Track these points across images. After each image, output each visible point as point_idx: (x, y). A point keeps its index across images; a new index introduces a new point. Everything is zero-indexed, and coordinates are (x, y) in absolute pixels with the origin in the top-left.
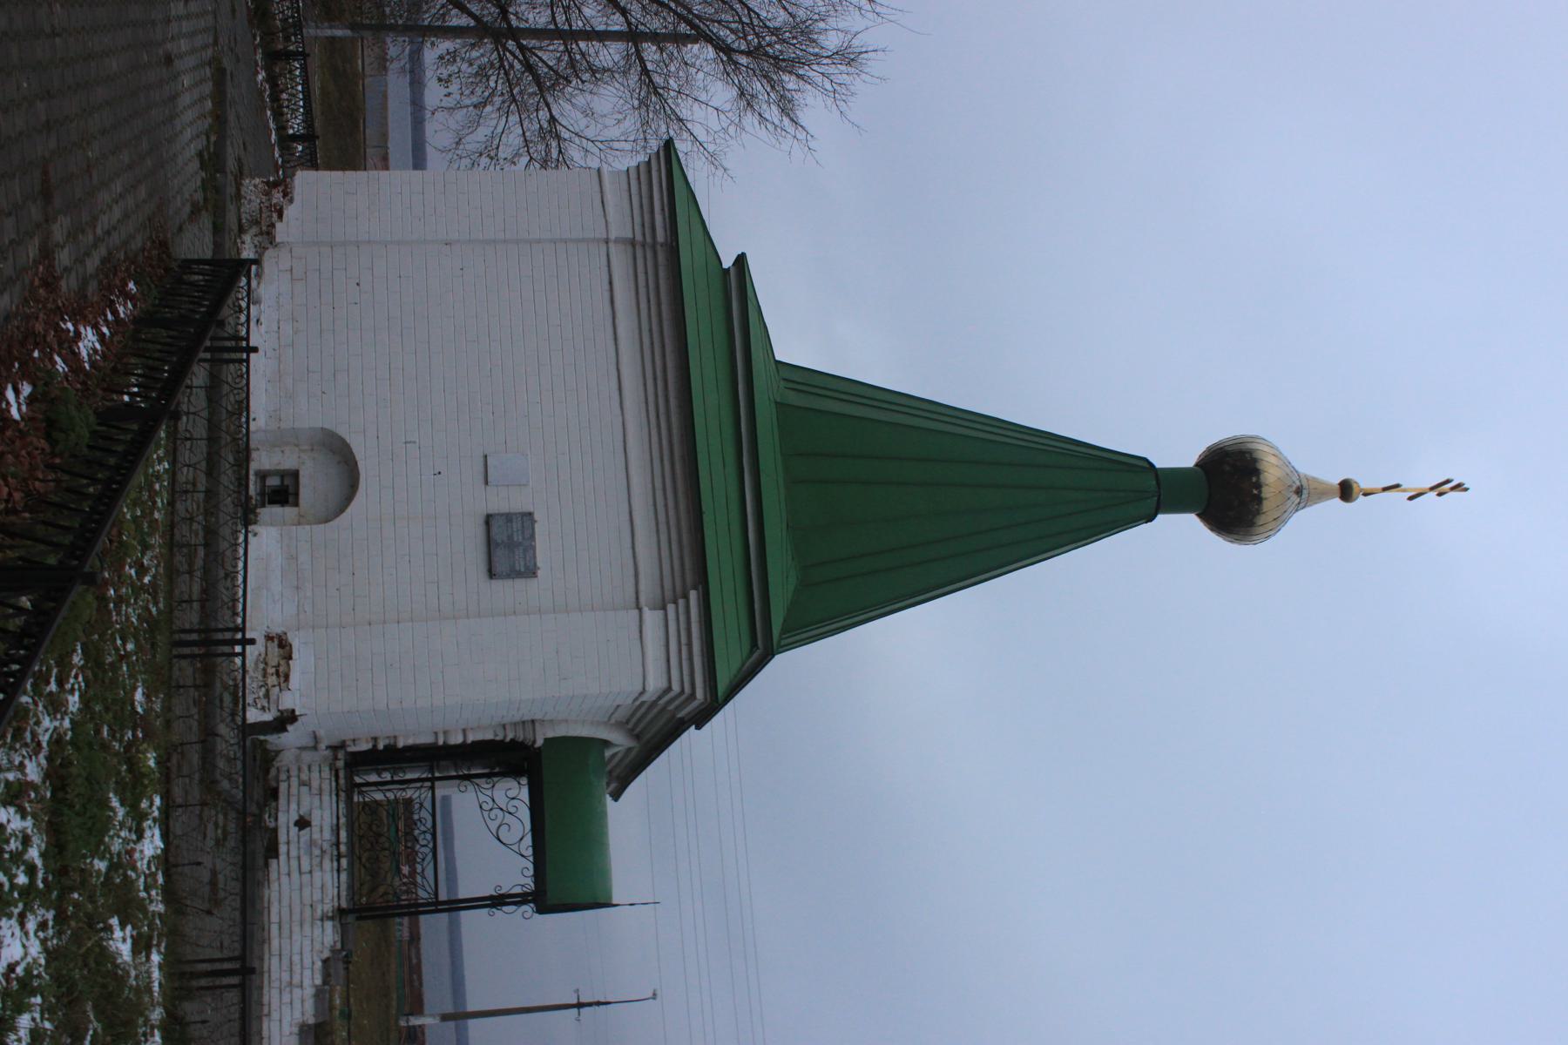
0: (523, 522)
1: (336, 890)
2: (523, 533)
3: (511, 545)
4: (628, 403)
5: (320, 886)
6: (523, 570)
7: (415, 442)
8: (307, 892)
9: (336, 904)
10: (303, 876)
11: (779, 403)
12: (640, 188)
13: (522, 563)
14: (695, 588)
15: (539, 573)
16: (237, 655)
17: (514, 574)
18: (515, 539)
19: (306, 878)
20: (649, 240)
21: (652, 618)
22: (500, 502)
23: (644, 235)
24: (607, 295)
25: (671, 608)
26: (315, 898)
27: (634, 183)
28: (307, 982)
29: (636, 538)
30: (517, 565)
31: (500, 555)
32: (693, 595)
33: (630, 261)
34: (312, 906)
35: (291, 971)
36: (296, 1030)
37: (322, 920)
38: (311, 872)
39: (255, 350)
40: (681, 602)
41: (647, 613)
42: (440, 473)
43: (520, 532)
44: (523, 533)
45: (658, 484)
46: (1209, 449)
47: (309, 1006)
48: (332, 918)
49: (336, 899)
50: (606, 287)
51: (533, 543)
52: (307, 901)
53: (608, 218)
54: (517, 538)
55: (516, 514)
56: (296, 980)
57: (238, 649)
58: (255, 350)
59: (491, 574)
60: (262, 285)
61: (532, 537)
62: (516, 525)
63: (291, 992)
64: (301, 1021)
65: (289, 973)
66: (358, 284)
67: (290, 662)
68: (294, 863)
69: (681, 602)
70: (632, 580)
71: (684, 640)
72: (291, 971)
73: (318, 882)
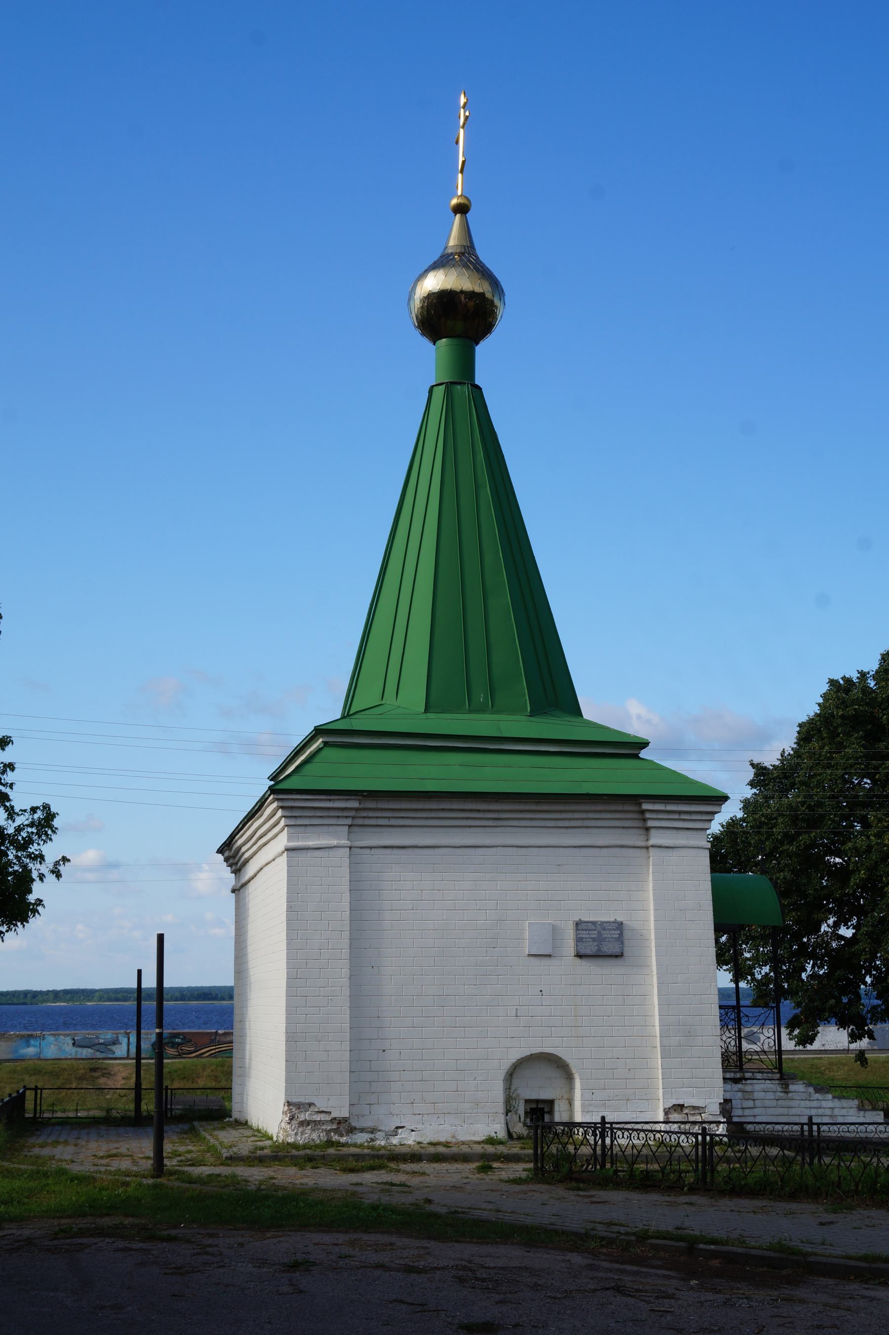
0: (583, 930)
1: (768, 1082)
2: (590, 930)
3: (600, 940)
4: (487, 842)
5: (764, 1093)
6: (619, 932)
7: (517, 1009)
8: (767, 1103)
9: (777, 1082)
10: (756, 1106)
11: (425, 710)
12: (306, 817)
13: (613, 932)
14: (640, 804)
15: (619, 919)
16: (819, 1129)
17: (620, 939)
18: (596, 936)
19: (758, 1103)
20: (352, 814)
21: (656, 838)
22: (569, 946)
23: (347, 817)
24: (396, 851)
25: (650, 824)
26: (773, 1097)
27: (299, 822)
28: (830, 1104)
29: (594, 845)
30: (615, 936)
31: (607, 948)
32: (645, 806)
33: (366, 829)
34: (777, 1100)
35: (821, 1116)
36: (862, 1113)
37: (787, 1093)
38: (754, 1100)
39: (603, 1118)
40: (648, 815)
41: (652, 842)
42: (541, 991)
43: (590, 932)
44: (590, 930)
45: (553, 824)
46: (423, 334)
47: (845, 1103)
48: (787, 1086)
49: (773, 1082)
50: (388, 851)
51: (599, 923)
52: (774, 1103)
53: (333, 845)
54: (594, 934)
55: (576, 935)
56: (828, 1112)
57: (815, 1128)
58: (603, 1118)
59: (619, 956)
60: (383, 1128)
61: (594, 923)
62: (584, 934)
63: (836, 1116)
64: (856, 1109)
65: (823, 1117)
66: (384, 1051)
67: (685, 1105)
68: (747, 1112)
69: (648, 815)
70: (624, 850)
71: (676, 816)
72: (821, 1116)
73: (761, 1095)
